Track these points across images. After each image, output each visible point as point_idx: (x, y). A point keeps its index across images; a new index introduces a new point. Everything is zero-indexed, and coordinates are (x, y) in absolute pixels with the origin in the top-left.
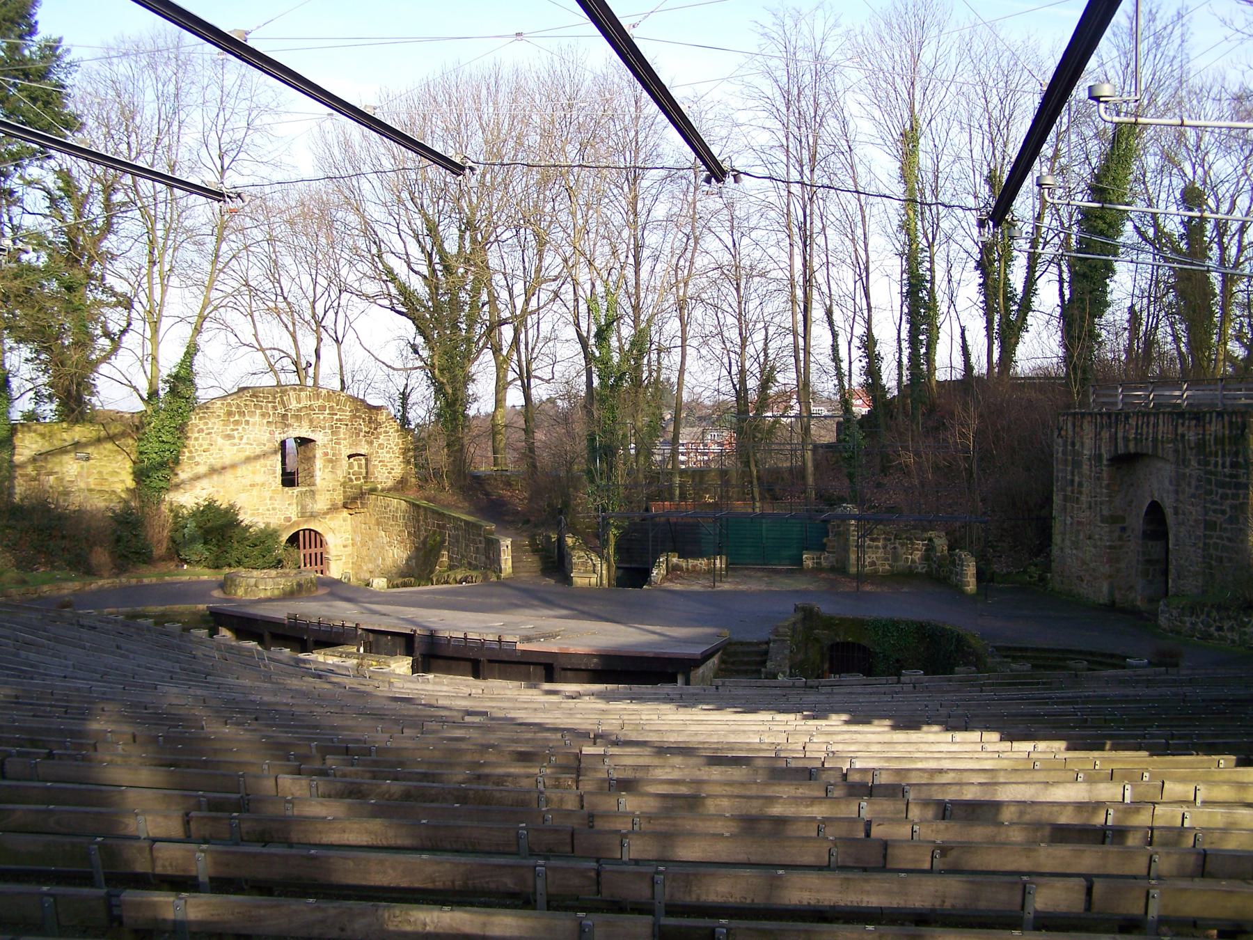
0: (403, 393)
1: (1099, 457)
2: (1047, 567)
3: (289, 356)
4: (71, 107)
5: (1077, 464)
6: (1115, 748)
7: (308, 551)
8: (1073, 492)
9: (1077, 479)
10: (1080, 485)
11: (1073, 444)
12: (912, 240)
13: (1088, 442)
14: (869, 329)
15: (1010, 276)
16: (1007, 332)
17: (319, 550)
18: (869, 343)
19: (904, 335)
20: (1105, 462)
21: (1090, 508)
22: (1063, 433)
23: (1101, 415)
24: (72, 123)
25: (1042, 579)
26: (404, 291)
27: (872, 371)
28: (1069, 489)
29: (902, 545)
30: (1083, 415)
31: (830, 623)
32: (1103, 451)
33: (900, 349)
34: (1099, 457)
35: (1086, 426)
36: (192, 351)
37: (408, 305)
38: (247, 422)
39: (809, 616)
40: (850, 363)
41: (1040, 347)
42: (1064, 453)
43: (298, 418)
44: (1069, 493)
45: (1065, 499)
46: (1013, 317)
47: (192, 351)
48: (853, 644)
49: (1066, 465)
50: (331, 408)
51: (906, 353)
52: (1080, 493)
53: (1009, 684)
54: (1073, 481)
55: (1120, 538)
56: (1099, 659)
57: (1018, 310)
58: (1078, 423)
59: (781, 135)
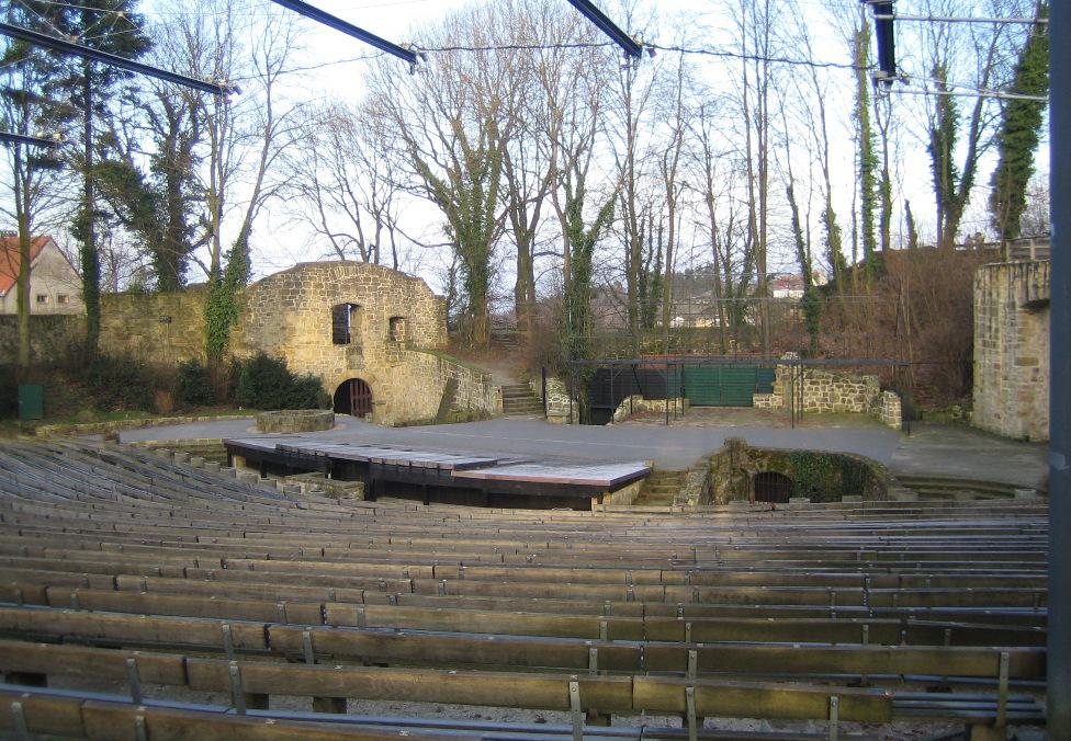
0: (452, 270)
1: (1012, 305)
2: (971, 408)
3: (355, 240)
4: (146, 32)
5: (994, 312)
6: (650, 675)
7: (357, 397)
8: (990, 337)
9: (994, 325)
10: (997, 331)
11: (990, 294)
12: (865, 125)
13: (1004, 293)
14: (829, 205)
15: (953, 154)
16: (951, 203)
17: (366, 396)
18: (829, 217)
19: (858, 208)
20: (1018, 309)
21: (1006, 351)
22: (982, 284)
23: (1014, 265)
24: (144, 45)
25: (965, 417)
26: (434, 181)
27: (833, 241)
28: (987, 335)
29: (839, 387)
30: (998, 267)
31: (754, 454)
32: (1016, 300)
33: (855, 221)
34: (1012, 305)
35: (1001, 277)
36: (247, 230)
37: (440, 196)
38: (304, 292)
39: (734, 447)
40: (808, 233)
41: (977, 217)
42: (983, 302)
43: (346, 288)
44: (987, 339)
45: (985, 344)
46: (956, 192)
47: (247, 230)
48: (776, 474)
49: (984, 313)
50: (375, 279)
51: (860, 224)
52: (997, 338)
53: (878, 512)
54: (990, 327)
55: (1034, 380)
56: (995, 489)
57: (961, 185)
58: (994, 275)
59: (738, 34)
